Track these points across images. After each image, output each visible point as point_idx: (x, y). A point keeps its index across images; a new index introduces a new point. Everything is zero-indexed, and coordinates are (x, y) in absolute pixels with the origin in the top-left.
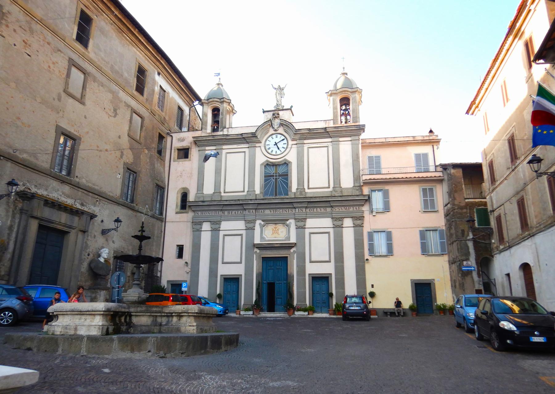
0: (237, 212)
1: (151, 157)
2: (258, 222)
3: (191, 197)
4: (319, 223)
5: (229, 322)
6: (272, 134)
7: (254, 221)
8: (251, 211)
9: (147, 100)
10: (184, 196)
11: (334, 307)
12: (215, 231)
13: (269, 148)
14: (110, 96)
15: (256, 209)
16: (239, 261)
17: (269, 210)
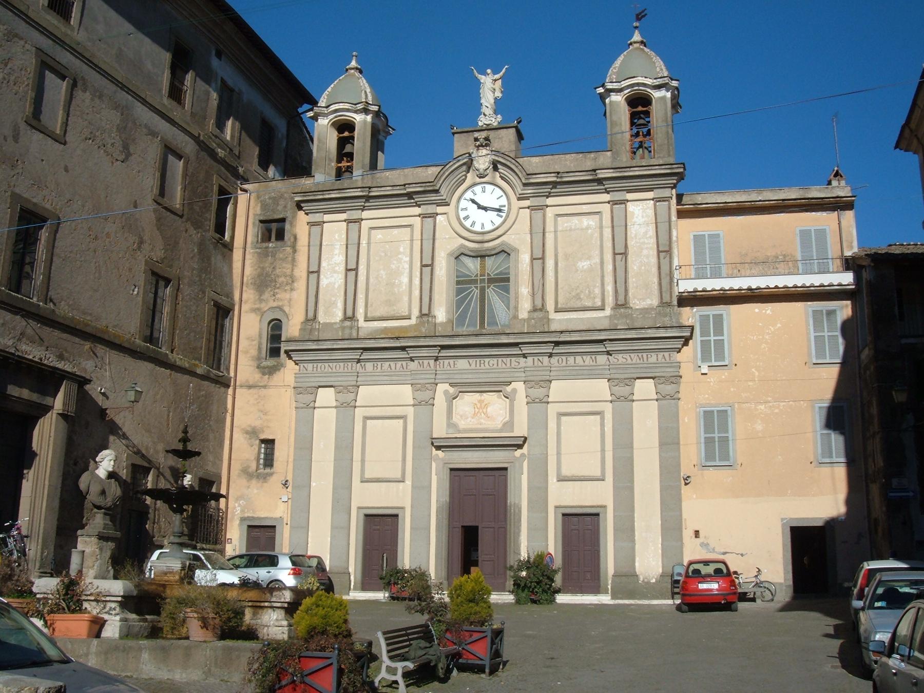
1: (201, 245)
2: (442, 388)
3: (292, 328)
4: (580, 390)
5: (73, 15)
6: (475, 185)
8: (426, 362)
10: (275, 329)
11: (381, 596)
12: (346, 407)
13: (467, 218)
14: (115, 117)
15: (437, 359)
17: (466, 361)
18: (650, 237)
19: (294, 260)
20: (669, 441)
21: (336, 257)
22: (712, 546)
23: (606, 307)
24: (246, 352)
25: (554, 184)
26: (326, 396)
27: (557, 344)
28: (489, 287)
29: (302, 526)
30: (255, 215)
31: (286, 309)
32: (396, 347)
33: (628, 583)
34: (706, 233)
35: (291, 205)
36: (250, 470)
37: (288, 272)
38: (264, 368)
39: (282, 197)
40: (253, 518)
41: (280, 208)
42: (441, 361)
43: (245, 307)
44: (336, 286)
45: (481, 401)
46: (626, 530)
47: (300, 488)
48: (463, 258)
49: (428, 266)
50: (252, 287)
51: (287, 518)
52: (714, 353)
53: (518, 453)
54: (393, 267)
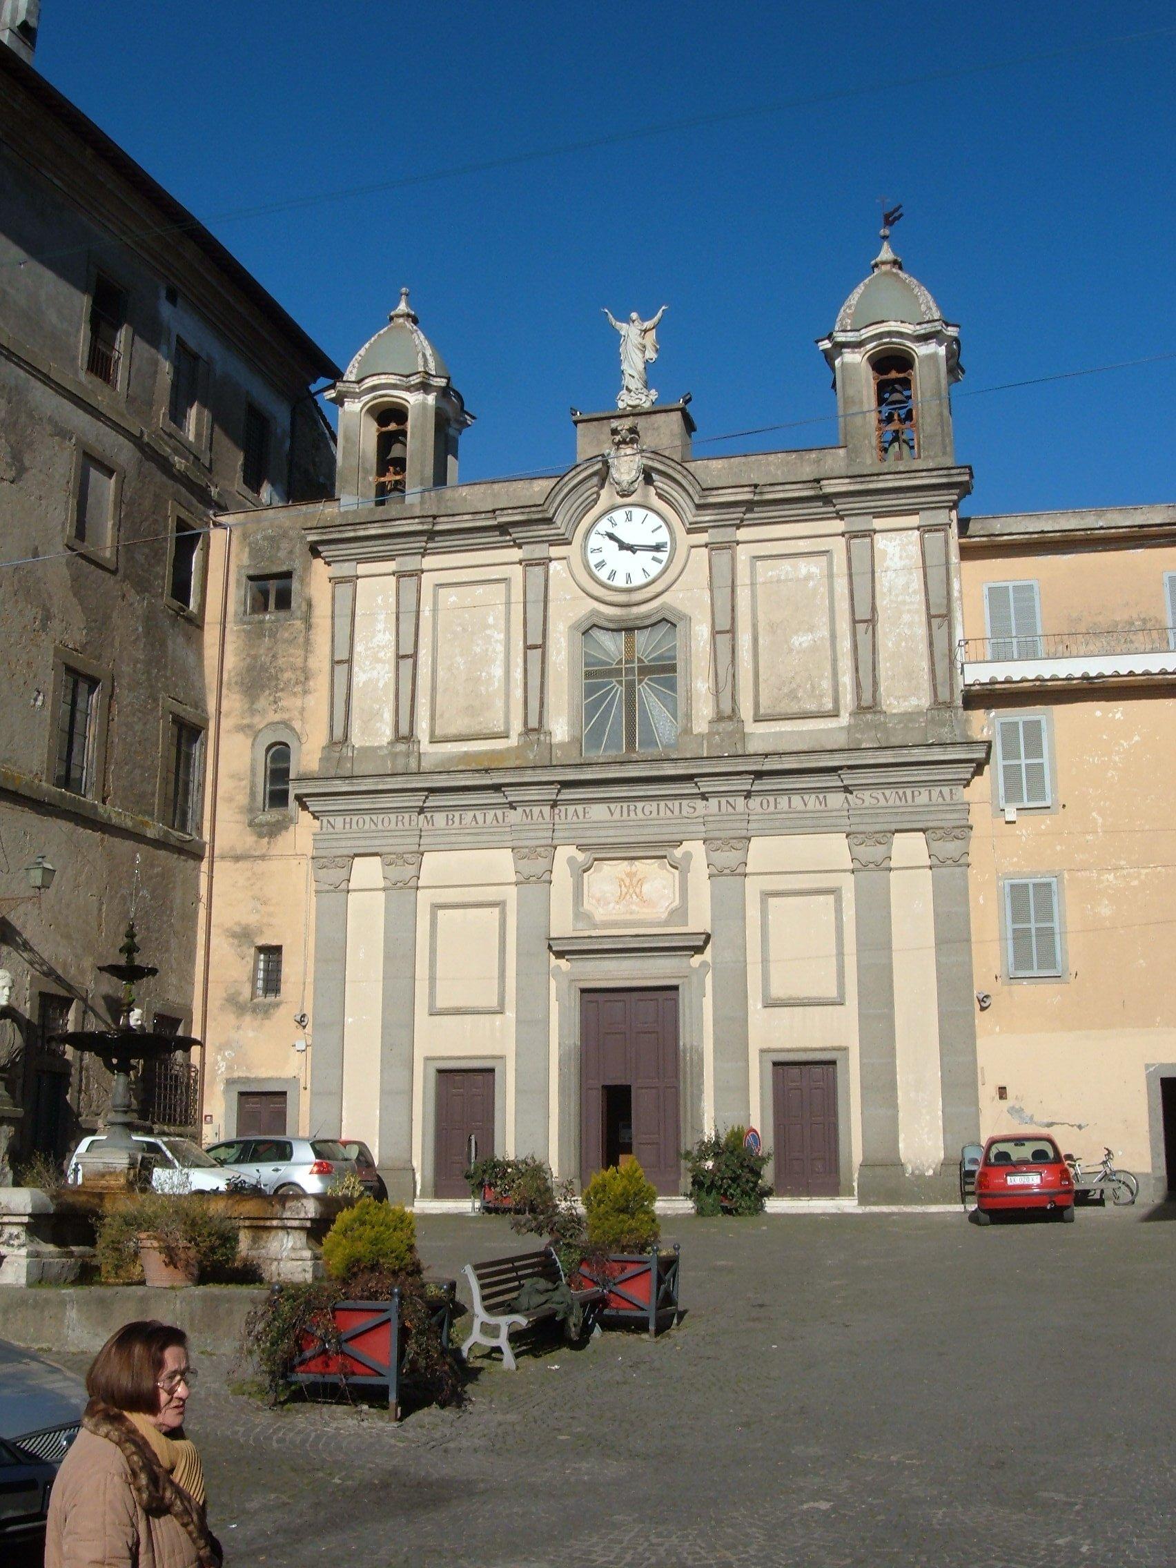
1: (150, 619)
2: (564, 853)
3: (308, 757)
4: (799, 853)
6: (614, 508)
8: (536, 810)
9: (130, 399)
12: (402, 888)
13: (601, 565)
16: (493, 1002)
18: (915, 592)
19: (307, 641)
20: (953, 936)
21: (380, 636)
22: (1028, 1112)
25: (750, 505)
26: (367, 871)
27: (759, 775)
28: (640, 681)
31: (297, 725)
32: (485, 785)
33: (886, 1177)
34: (1011, 585)
35: (300, 549)
36: (241, 999)
37: (299, 662)
38: (261, 825)
39: (284, 535)
40: (248, 1080)
41: (282, 554)
42: (563, 808)
44: (381, 685)
45: (631, 875)
46: (882, 1087)
47: (326, 1027)
49: (537, 647)
50: (237, 688)
51: (305, 1079)
52: (1027, 787)
53: (696, 960)
54: (478, 650)
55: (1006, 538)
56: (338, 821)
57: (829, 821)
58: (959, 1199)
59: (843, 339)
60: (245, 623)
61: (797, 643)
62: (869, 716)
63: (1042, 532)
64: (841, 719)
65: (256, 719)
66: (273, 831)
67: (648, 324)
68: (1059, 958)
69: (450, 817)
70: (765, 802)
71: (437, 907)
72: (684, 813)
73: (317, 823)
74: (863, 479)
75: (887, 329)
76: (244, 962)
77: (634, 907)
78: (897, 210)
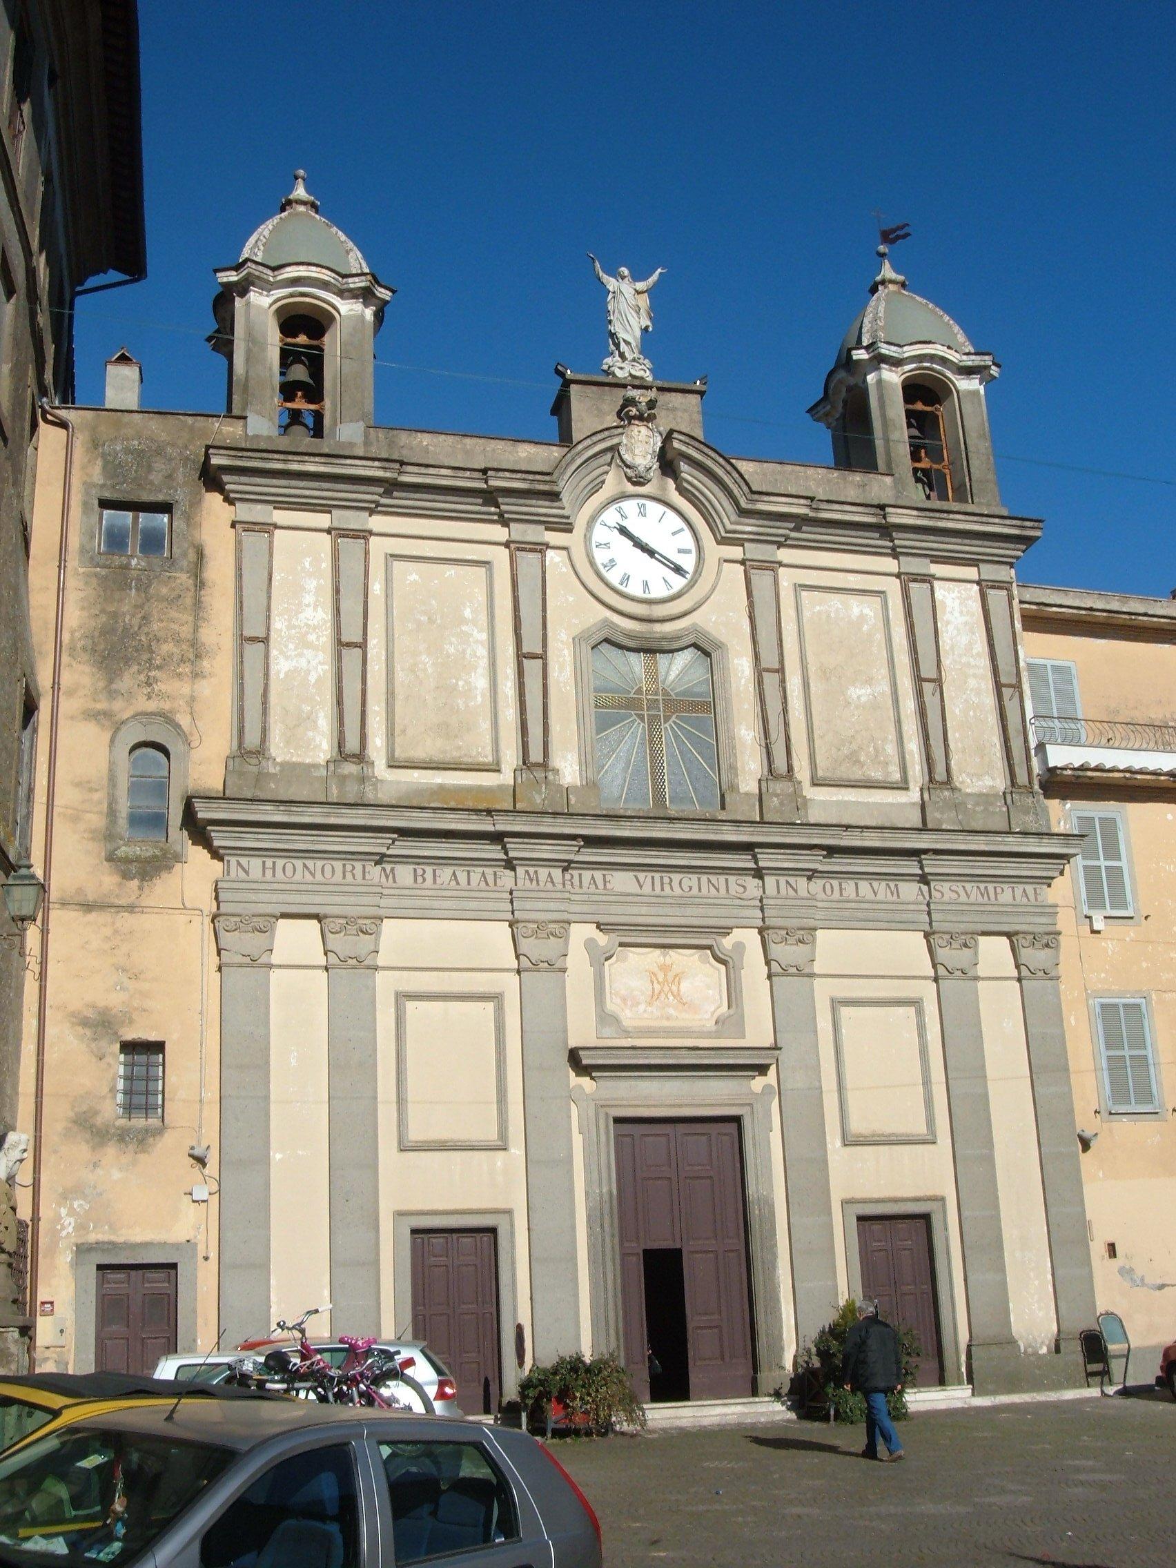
0: (462, 877)
2: (581, 933)
3: (205, 766)
4: (868, 952)
6: (624, 496)
7: (559, 929)
8: (543, 873)
16: (492, 1135)
18: (978, 654)
19: (198, 605)
20: (1047, 1063)
21: (309, 612)
22: (1139, 1273)
23: (911, 785)
24: (75, 819)
25: (800, 522)
26: (297, 940)
27: (832, 851)
28: (667, 719)
29: (247, 1259)
30: (88, 486)
31: (184, 720)
32: (487, 833)
33: (996, 1361)
34: (1049, 663)
35: (186, 476)
36: (99, 1121)
37: (186, 631)
38: (127, 861)
39: (160, 451)
40: (113, 1246)
41: (156, 478)
42: (576, 873)
43: (67, 706)
44: (313, 678)
45: (665, 968)
46: (987, 1246)
47: (238, 1168)
48: (605, 648)
49: (530, 657)
50: (86, 657)
51: (208, 1243)
52: (1107, 889)
53: (758, 1083)
54: (452, 650)
55: (1054, 609)
56: (255, 864)
57: (906, 916)
58: (1083, 1381)
59: (887, 352)
60: (97, 565)
61: (854, 696)
62: (947, 793)
63: (1091, 609)
64: (910, 793)
65: (118, 705)
66: (149, 868)
67: (641, 286)
68: (1155, 1091)
69: (420, 872)
70: (828, 886)
71: (402, 997)
72: (732, 892)
73: (218, 865)
74: (931, 514)
75: (933, 352)
76: (103, 1064)
77: (671, 1011)
78: (901, 228)
